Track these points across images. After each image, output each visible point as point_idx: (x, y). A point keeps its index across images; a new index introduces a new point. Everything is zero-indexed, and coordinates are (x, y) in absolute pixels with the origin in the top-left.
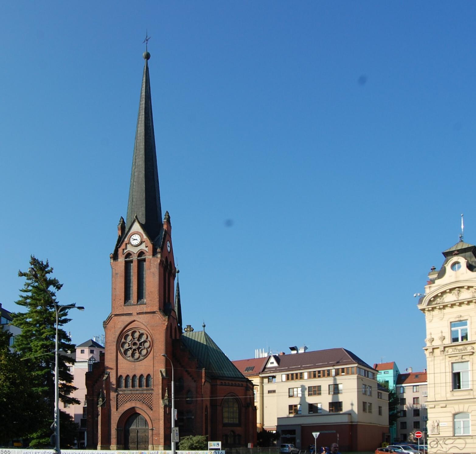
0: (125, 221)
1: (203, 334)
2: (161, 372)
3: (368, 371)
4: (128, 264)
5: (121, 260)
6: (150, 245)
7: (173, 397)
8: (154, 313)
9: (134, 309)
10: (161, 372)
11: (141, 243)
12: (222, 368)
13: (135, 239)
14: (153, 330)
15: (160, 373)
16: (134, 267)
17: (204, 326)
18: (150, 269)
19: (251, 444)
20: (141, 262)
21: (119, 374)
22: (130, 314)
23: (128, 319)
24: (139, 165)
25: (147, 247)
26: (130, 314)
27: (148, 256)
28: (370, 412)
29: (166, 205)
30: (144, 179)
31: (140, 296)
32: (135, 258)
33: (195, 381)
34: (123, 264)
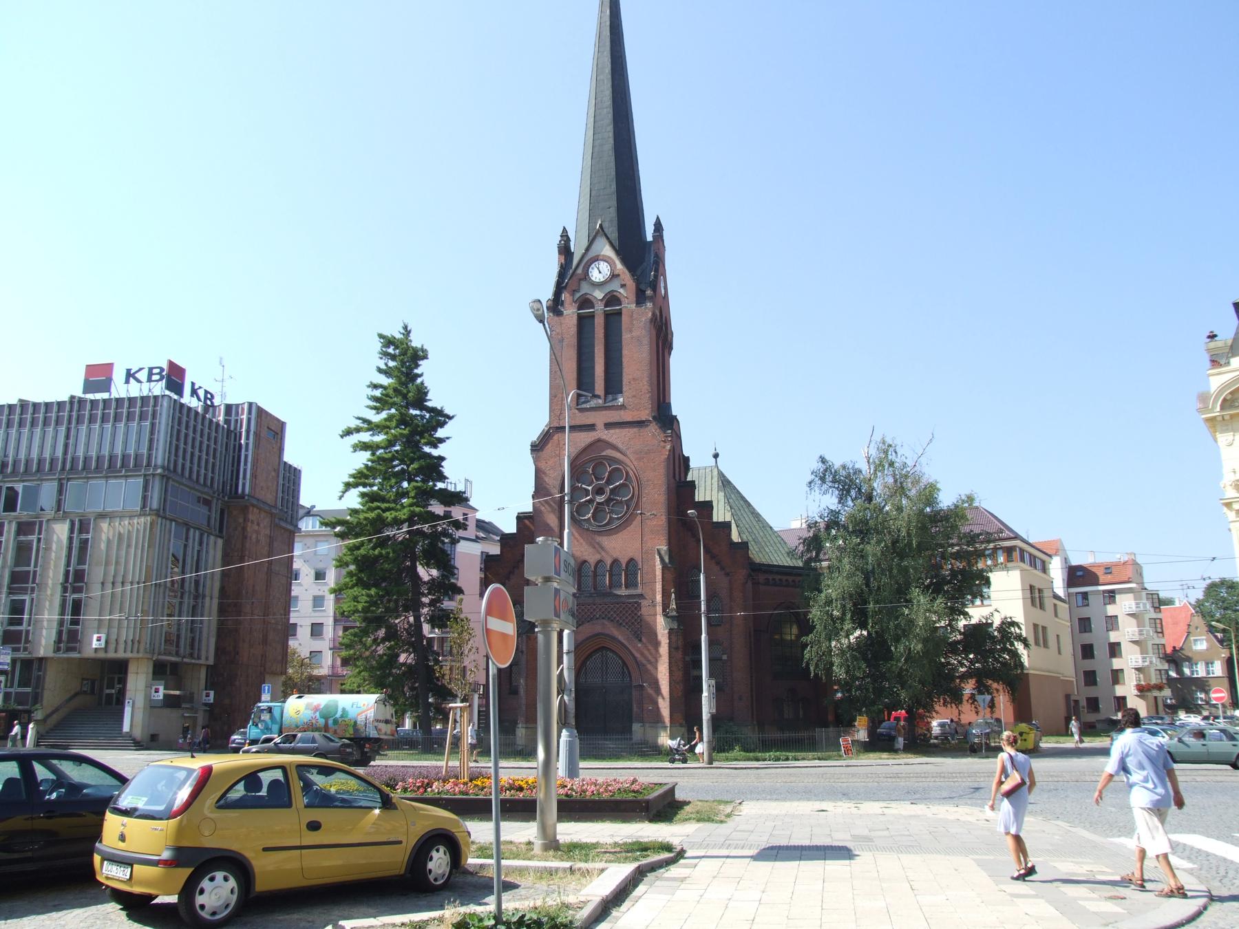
0: (572, 235)
1: (715, 473)
2: (659, 551)
3: (191, 656)
4: (584, 323)
5: (570, 312)
6: (631, 283)
7: (703, 608)
8: (640, 424)
9: (599, 419)
10: (659, 551)
11: (614, 276)
12: (130, 643)
13: (599, 273)
14: (639, 459)
15: (657, 557)
16: (599, 322)
17: (716, 456)
18: (631, 331)
19: (371, 714)
20: (613, 319)
21: (1029, 865)
22: (591, 427)
23: (585, 438)
24: (142, 417)
25: (623, 286)
26: (591, 427)
27: (628, 305)
28: (1046, 645)
29: (655, 203)
30: (612, 153)
31: (613, 385)
32: (599, 308)
33: (727, 574)
34: (574, 320)
